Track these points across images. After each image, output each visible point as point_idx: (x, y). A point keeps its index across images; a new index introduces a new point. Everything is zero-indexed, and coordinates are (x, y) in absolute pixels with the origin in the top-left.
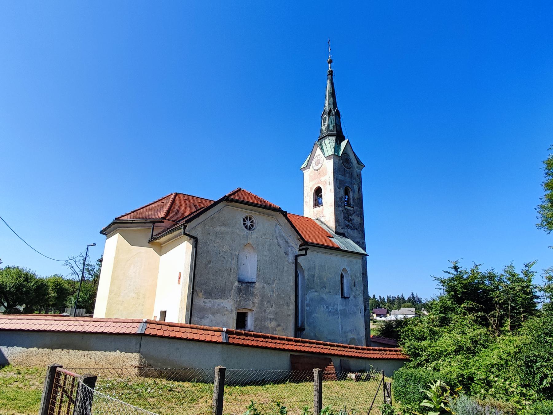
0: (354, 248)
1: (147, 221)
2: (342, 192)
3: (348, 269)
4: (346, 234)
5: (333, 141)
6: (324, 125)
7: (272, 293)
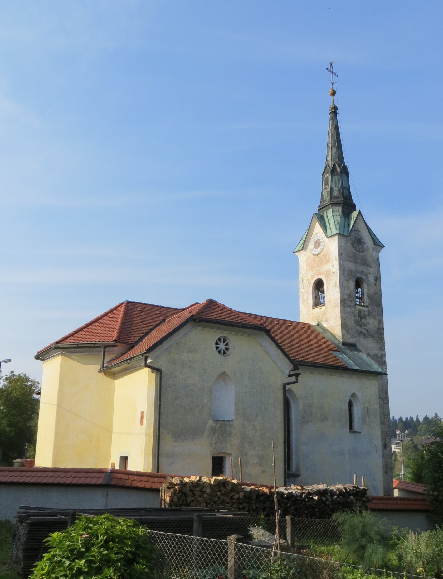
0: (368, 365)
1: (96, 345)
2: (352, 285)
3: (359, 394)
4: (358, 346)
5: (338, 214)
6: (325, 189)
7: (254, 432)
